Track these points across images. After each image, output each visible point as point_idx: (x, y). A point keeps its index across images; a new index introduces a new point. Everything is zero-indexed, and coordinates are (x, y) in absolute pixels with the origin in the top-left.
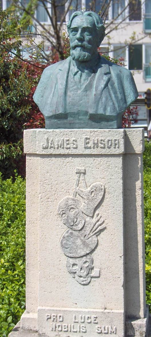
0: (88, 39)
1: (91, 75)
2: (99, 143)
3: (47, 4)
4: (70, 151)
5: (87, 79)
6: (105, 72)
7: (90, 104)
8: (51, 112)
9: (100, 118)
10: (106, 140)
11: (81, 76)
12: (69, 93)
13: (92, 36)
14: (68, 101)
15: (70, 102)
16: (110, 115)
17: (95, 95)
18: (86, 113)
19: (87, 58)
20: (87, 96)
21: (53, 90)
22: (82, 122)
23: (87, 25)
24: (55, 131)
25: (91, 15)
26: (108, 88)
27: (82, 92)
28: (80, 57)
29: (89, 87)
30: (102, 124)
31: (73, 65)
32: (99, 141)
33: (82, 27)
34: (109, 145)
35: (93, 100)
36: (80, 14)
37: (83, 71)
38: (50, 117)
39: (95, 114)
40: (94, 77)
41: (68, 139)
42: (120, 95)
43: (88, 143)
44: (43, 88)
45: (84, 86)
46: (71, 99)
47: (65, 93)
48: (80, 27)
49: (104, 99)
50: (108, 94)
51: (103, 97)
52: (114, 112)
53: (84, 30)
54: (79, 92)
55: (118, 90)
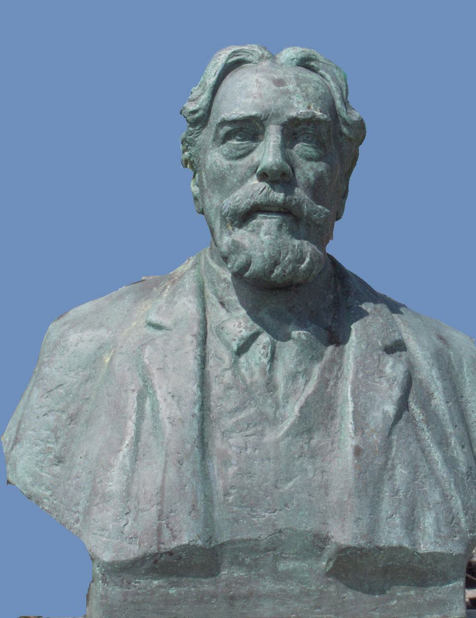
0: (312, 179)
1: (322, 355)
5: (307, 373)
7: (334, 496)
8: (133, 538)
9: (386, 571)
11: (273, 358)
12: (218, 444)
13: (327, 163)
14: (219, 485)
15: (232, 487)
16: (439, 550)
17: (358, 451)
18: (318, 542)
19: (309, 269)
20: (313, 457)
21: (131, 426)
22: (294, 588)
23: (309, 108)
25: (312, 64)
26: (412, 420)
27: (287, 434)
28: (276, 263)
29: (319, 414)
30: (392, 597)
31: (222, 304)
35: (351, 478)
36: (261, 58)
37: (280, 335)
39: (367, 546)
40: (336, 363)
42: (460, 452)
44: (64, 417)
45: (297, 409)
46: (236, 474)
47: (203, 441)
48: (277, 115)
49: (401, 472)
50: (414, 447)
51: (396, 461)
52: (452, 535)
53: (294, 130)
54: (271, 436)
55: (450, 430)
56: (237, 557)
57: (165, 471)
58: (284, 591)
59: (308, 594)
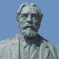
1: (37, 48)
5: (34, 51)
6: (46, 46)
19: (35, 36)
28: (30, 35)
31: (22, 41)
33: (31, 14)
36: (28, 5)
40: (39, 49)
53: (33, 15)
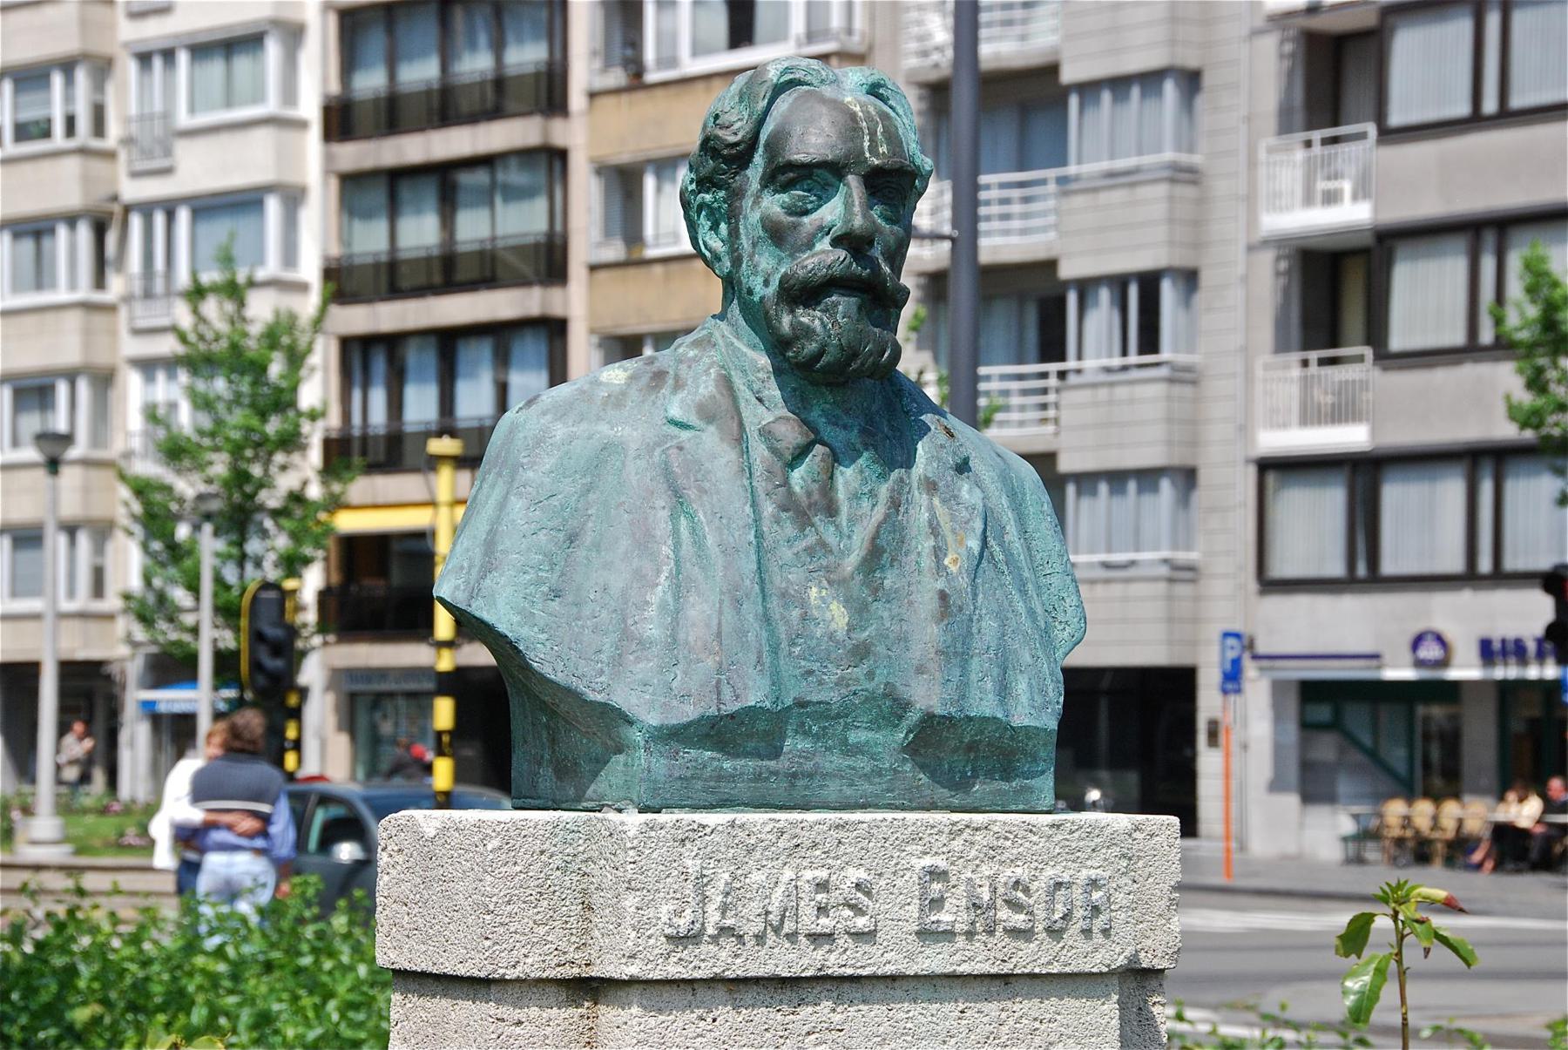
2: (999, 902)
3: (536, 38)
4: (832, 957)
10: (1040, 886)
24: (742, 826)
28: (855, 355)
31: (760, 400)
32: (1001, 890)
34: (1057, 916)
38: (674, 736)
41: (823, 874)
43: (937, 903)
44: (561, 536)
56: (803, 724)
57: (720, 612)
58: (854, 769)
59: (879, 773)
